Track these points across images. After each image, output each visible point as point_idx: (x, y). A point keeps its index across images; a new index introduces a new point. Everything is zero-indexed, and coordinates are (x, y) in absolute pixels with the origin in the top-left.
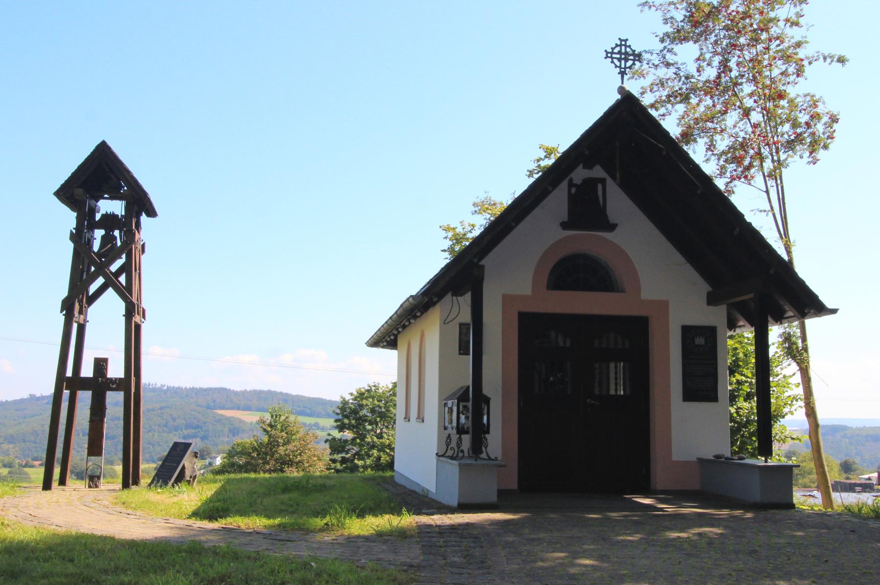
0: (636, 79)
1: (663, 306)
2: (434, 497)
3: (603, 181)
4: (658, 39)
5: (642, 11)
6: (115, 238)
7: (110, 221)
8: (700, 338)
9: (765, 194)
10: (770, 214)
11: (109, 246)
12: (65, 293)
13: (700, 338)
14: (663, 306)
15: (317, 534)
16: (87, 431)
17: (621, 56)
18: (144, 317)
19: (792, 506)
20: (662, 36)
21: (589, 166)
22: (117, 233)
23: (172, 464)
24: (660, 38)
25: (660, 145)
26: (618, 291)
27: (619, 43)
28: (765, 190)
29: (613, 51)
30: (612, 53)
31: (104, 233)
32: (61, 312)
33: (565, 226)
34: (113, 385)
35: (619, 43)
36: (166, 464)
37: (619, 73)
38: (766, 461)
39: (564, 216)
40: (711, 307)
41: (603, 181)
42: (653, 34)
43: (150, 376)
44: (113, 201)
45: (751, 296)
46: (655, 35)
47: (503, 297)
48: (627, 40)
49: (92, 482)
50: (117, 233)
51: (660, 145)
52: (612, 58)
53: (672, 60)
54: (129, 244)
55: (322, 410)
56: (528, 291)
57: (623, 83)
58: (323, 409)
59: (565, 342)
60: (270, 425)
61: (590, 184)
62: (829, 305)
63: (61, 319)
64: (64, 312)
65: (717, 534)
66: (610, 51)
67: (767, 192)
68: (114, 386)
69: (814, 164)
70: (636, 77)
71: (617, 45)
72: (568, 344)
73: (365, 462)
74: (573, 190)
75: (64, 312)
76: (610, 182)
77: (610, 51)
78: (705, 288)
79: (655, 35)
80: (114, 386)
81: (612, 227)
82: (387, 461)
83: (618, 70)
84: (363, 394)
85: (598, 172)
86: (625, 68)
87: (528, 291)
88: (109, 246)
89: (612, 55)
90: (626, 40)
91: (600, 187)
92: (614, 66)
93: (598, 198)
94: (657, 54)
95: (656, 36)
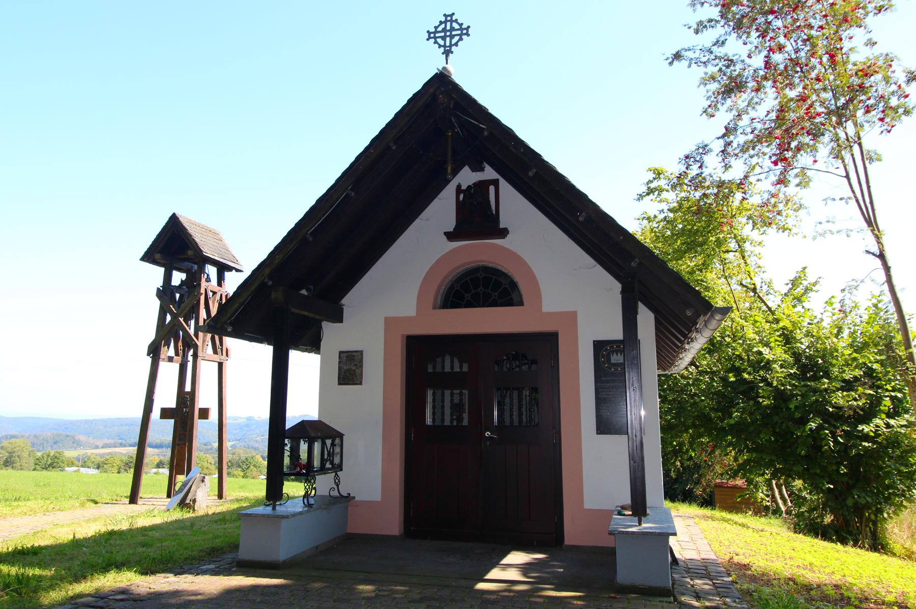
1: (571, 318)
3: (495, 183)
4: (692, 30)
8: (617, 354)
9: (845, 180)
13: (617, 354)
14: (571, 318)
16: (266, 454)
17: (448, 36)
18: (227, 355)
20: (695, 26)
21: (477, 167)
24: (694, 29)
25: (481, 125)
29: (436, 30)
30: (435, 33)
33: (450, 236)
37: (443, 53)
39: (451, 226)
40: (344, 319)
41: (495, 183)
42: (685, 26)
46: (687, 27)
47: (385, 320)
51: (481, 125)
53: (720, 52)
57: (447, 63)
59: (461, 367)
61: (482, 186)
63: (149, 360)
64: (151, 355)
65: (582, 605)
66: (433, 30)
67: (847, 177)
72: (465, 368)
75: (151, 355)
76: (504, 185)
77: (433, 30)
79: (687, 27)
81: (504, 233)
83: (442, 49)
86: (451, 46)
89: (435, 35)
91: (492, 189)
92: (438, 46)
93: (489, 202)
94: (701, 50)
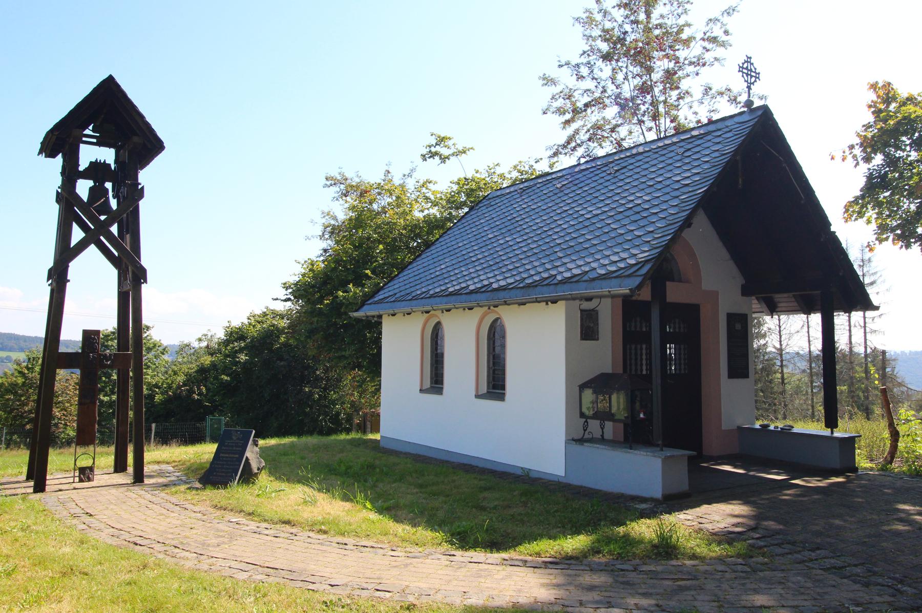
0: (549, 86)
1: (714, 295)
2: (564, 481)
6: (107, 190)
7: (97, 171)
11: (103, 200)
14: (714, 295)
19: (855, 470)
22: (109, 185)
23: (232, 456)
26: (680, 281)
31: (107, 183)
34: (107, 361)
36: (222, 455)
38: (832, 433)
44: (101, 147)
45: (819, 292)
49: (84, 475)
50: (109, 185)
51: (780, 158)
52: (743, 73)
54: (136, 199)
55: (14, 345)
58: (16, 344)
60: (27, 368)
62: (875, 302)
68: (109, 363)
70: (549, 84)
71: (746, 62)
73: (111, 398)
78: (740, 280)
80: (109, 363)
82: (161, 400)
84: (109, 336)
88: (103, 200)
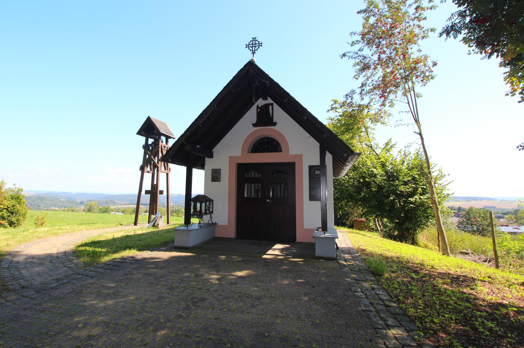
1: (300, 157)
3: (272, 104)
5: (352, 37)
9: (408, 104)
10: (410, 113)
12: (141, 163)
14: (300, 157)
15: (513, 301)
20: (351, 43)
27: (248, 48)
28: (407, 102)
32: (140, 170)
33: (254, 125)
35: (248, 48)
39: (254, 121)
41: (272, 104)
43: (171, 192)
48: (262, 46)
56: (239, 154)
59: (258, 175)
61: (267, 106)
63: (140, 172)
67: (408, 103)
69: (425, 85)
74: (259, 110)
81: (275, 124)
85: (270, 101)
87: (239, 154)
90: (261, 46)
91: (270, 107)
95: (349, 44)
